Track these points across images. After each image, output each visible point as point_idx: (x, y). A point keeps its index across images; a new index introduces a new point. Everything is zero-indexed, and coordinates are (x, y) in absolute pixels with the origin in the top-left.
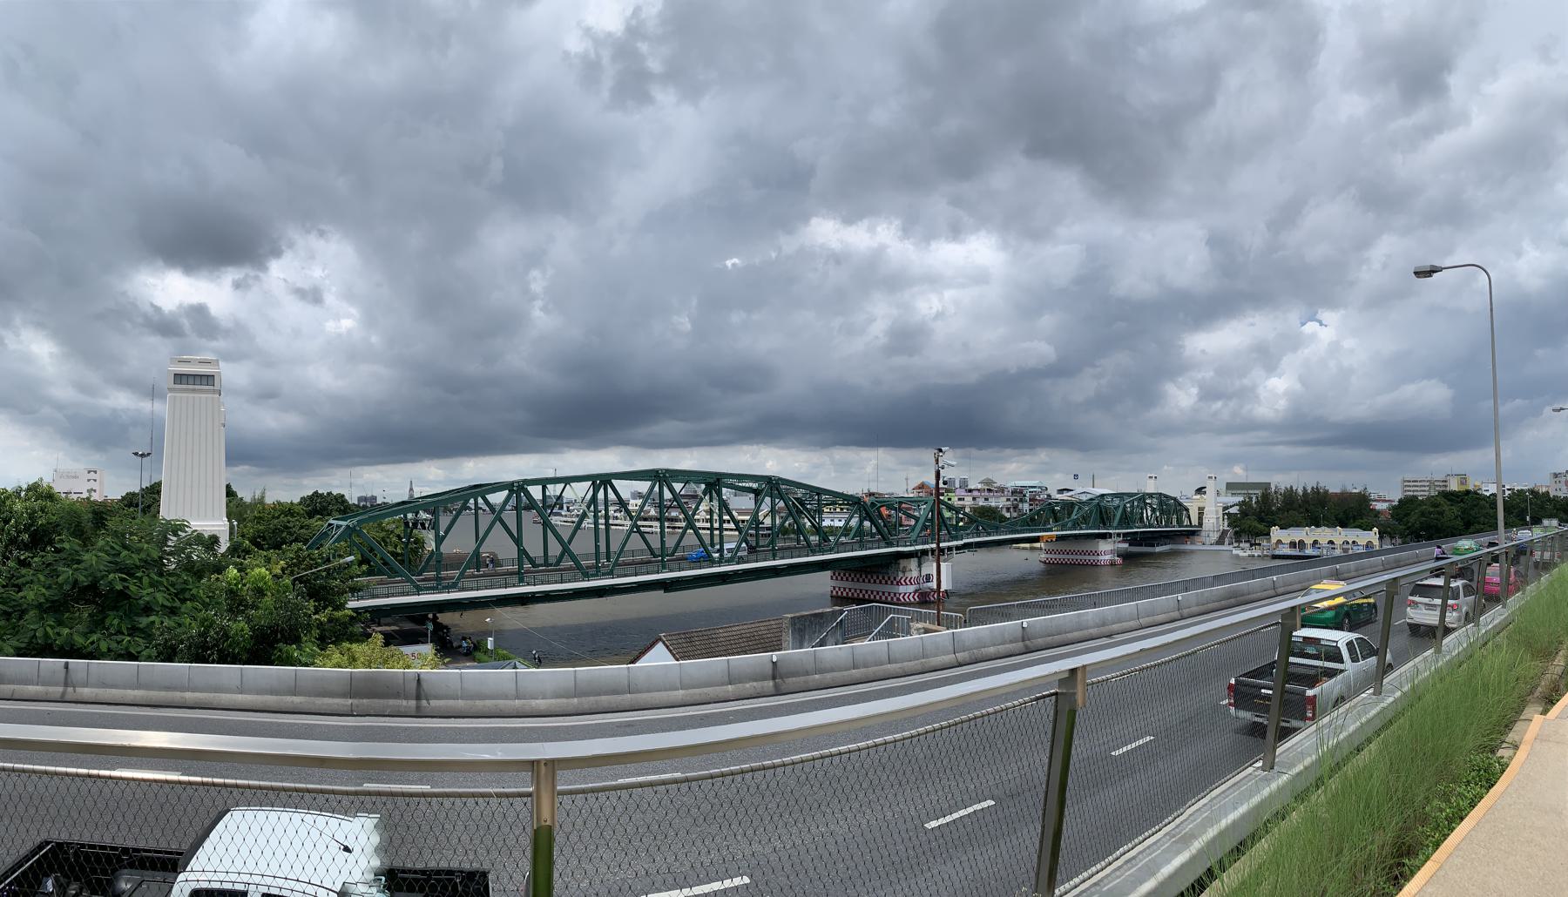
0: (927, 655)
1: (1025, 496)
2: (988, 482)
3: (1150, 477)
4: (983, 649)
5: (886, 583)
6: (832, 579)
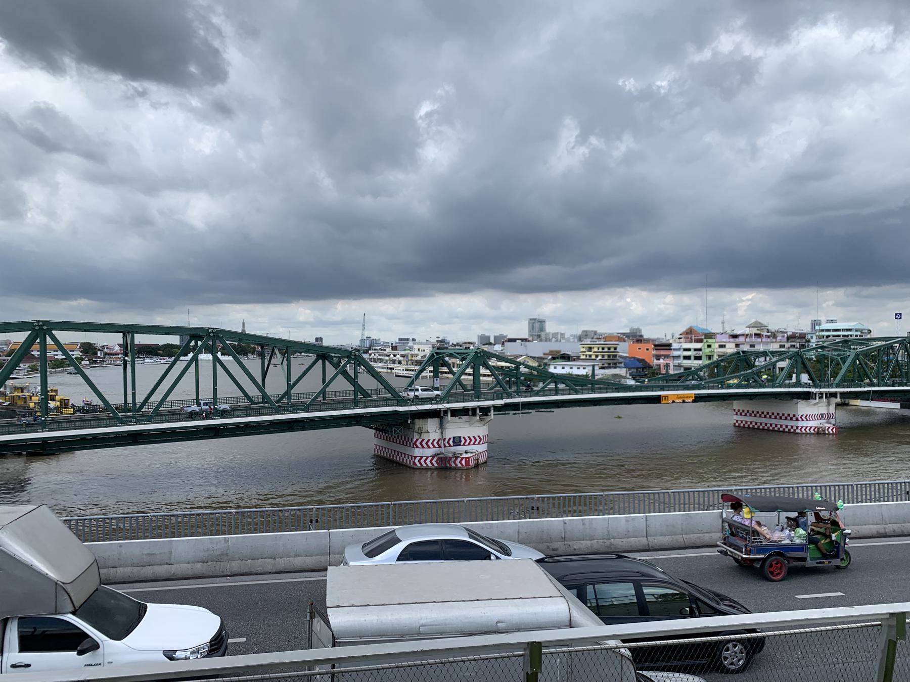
1: (808, 341)
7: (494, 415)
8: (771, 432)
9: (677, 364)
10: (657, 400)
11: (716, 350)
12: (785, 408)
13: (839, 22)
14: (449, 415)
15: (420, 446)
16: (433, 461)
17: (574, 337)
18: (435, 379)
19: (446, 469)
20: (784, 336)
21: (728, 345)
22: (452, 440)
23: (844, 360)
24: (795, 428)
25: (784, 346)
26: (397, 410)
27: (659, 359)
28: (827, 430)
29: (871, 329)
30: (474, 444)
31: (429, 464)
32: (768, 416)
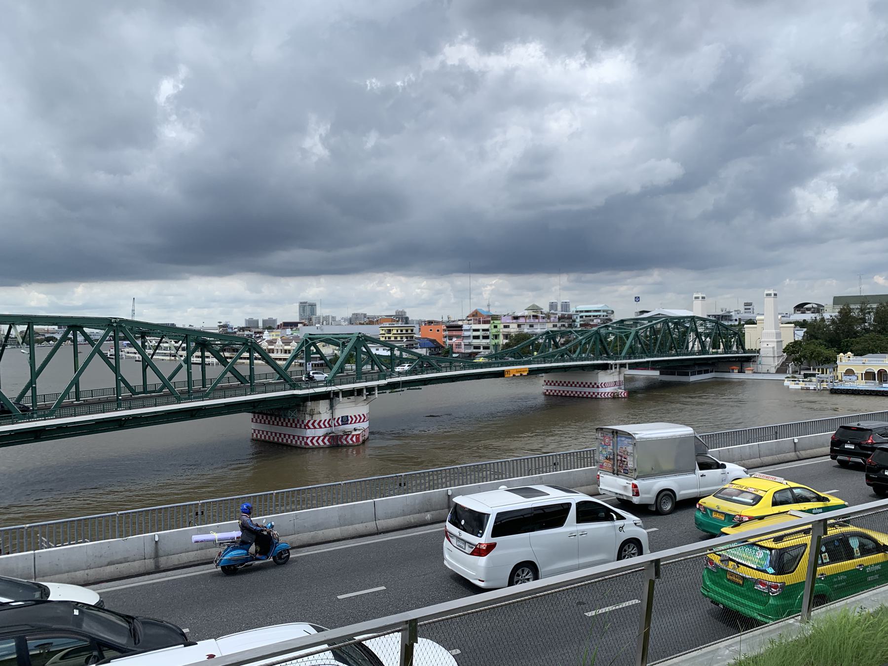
1: (574, 321)
2: (535, 308)
3: (697, 298)
5: (296, 426)
6: (252, 421)
7: (378, 393)
8: (572, 398)
9: (468, 344)
10: (501, 374)
11: (501, 330)
12: (588, 378)
14: (341, 396)
15: (312, 427)
16: (313, 441)
17: (345, 320)
18: (308, 363)
19: (338, 446)
20: (555, 317)
21: (511, 326)
22: (340, 419)
23: (627, 337)
24: (596, 394)
25: (556, 325)
26: (294, 393)
27: (451, 339)
28: (621, 394)
29: (614, 310)
30: (359, 422)
31: (322, 444)
32: (573, 385)
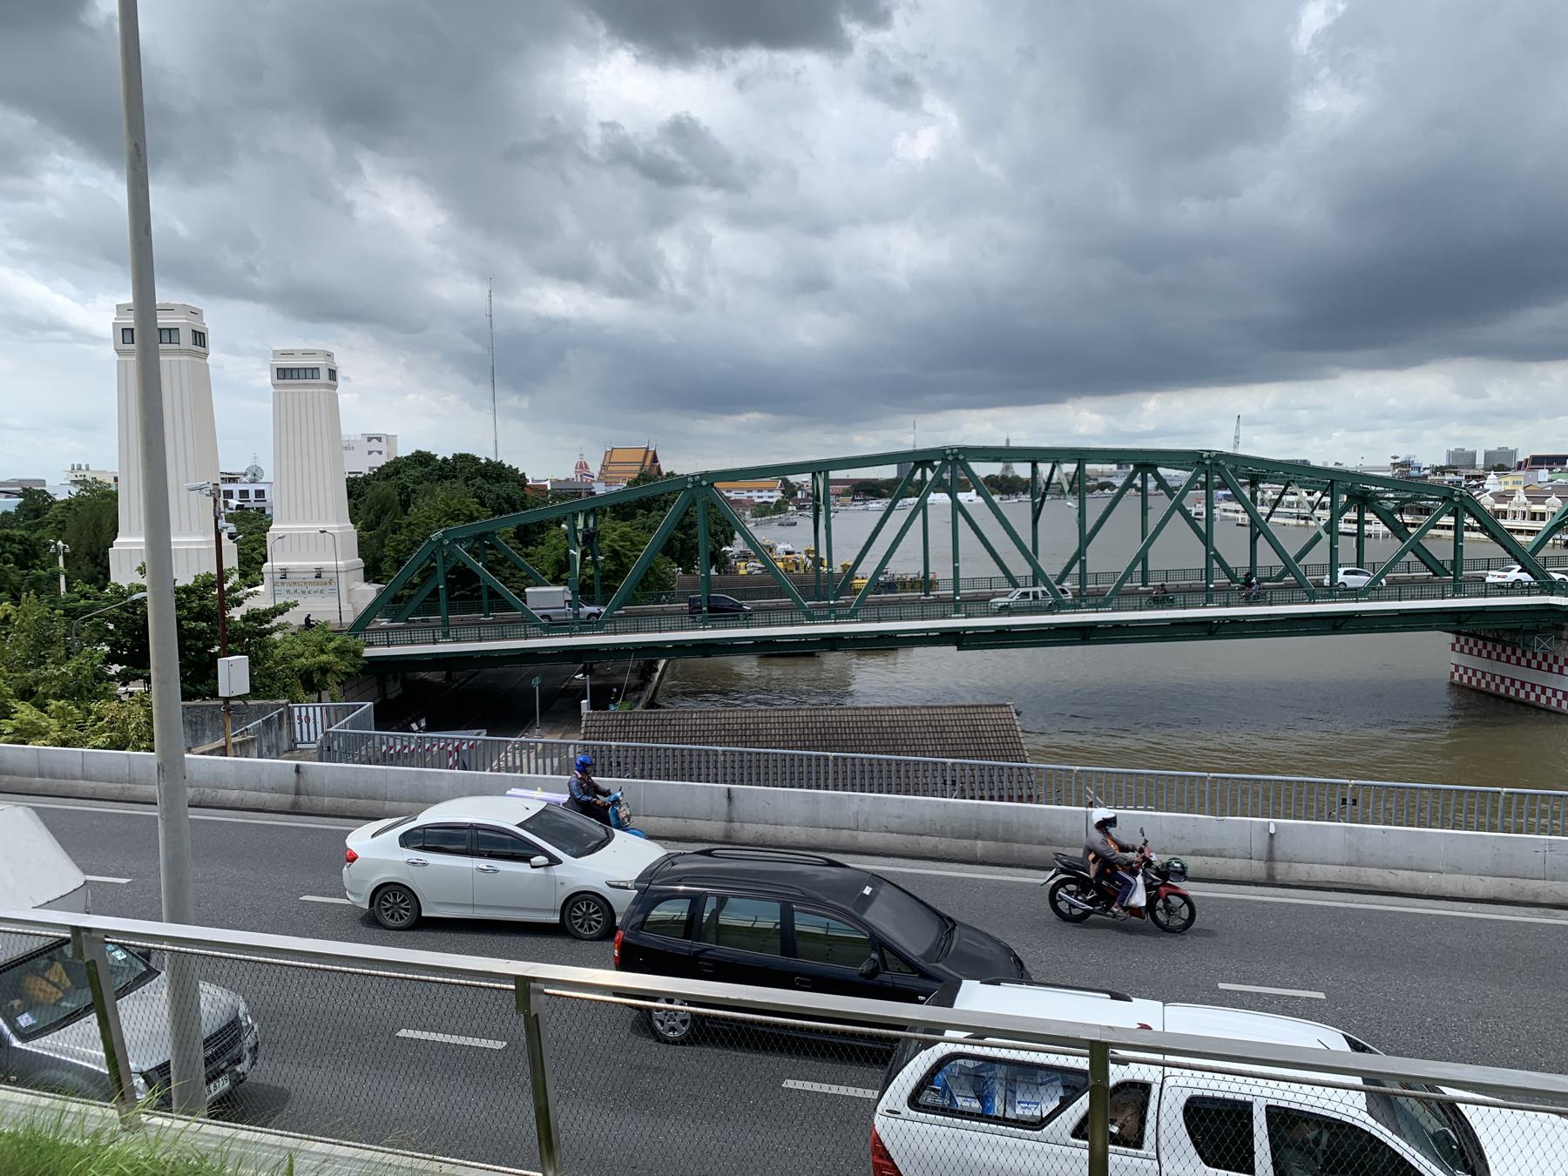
0: (134, 779)
4: (221, 791)
5: (1550, 670)
6: (1453, 649)
13: (477, 348)
